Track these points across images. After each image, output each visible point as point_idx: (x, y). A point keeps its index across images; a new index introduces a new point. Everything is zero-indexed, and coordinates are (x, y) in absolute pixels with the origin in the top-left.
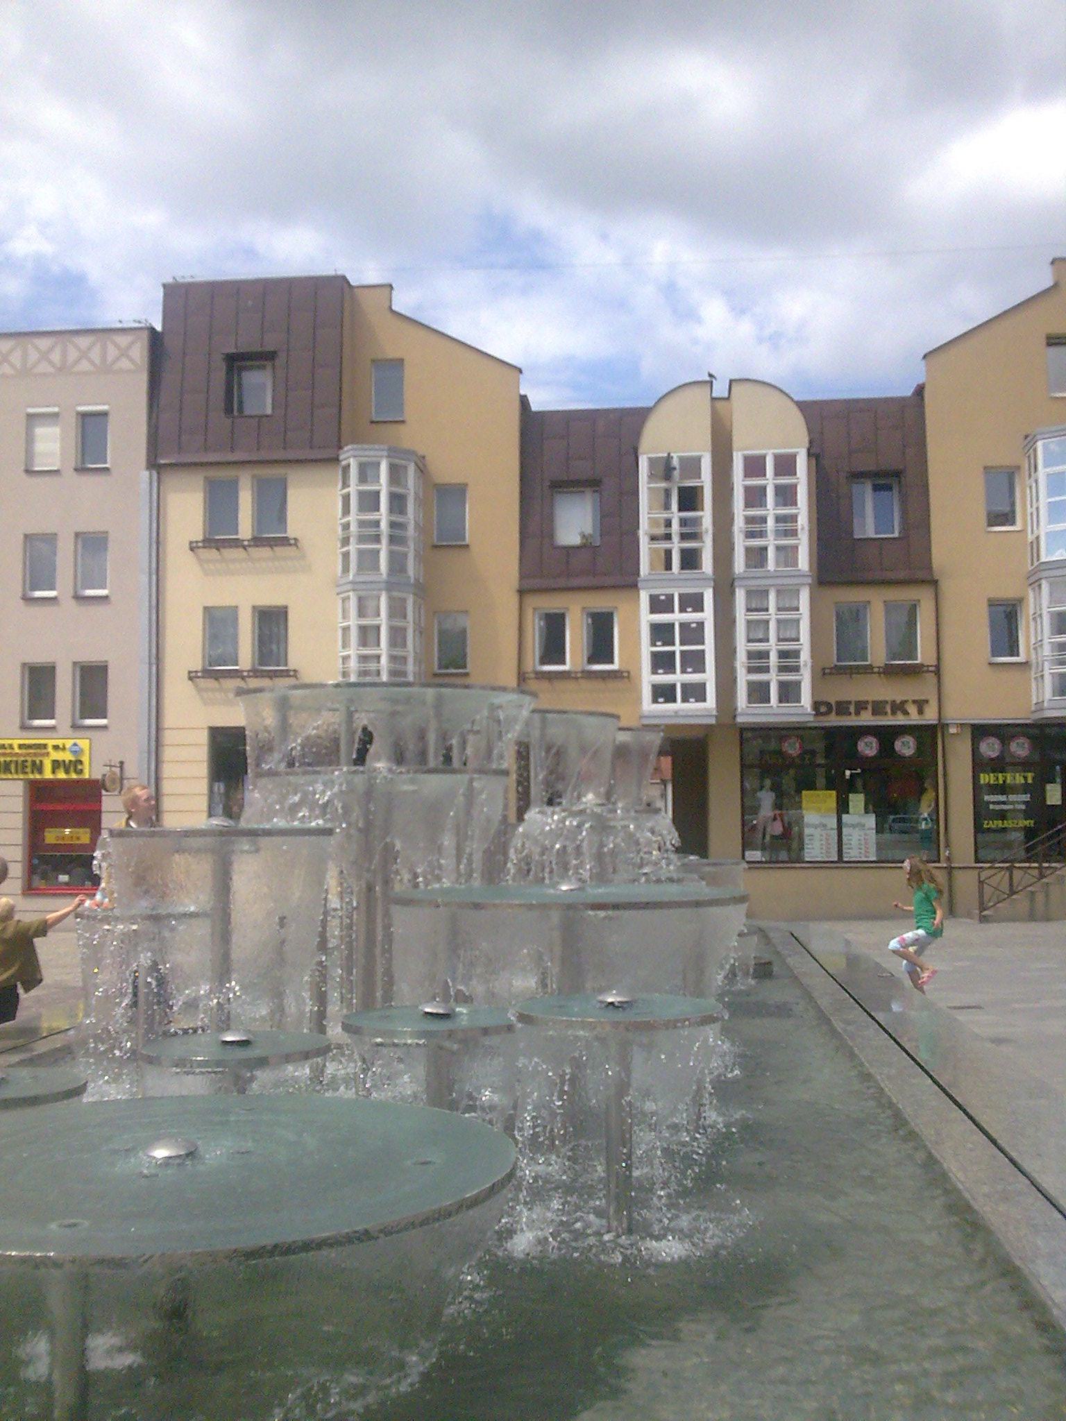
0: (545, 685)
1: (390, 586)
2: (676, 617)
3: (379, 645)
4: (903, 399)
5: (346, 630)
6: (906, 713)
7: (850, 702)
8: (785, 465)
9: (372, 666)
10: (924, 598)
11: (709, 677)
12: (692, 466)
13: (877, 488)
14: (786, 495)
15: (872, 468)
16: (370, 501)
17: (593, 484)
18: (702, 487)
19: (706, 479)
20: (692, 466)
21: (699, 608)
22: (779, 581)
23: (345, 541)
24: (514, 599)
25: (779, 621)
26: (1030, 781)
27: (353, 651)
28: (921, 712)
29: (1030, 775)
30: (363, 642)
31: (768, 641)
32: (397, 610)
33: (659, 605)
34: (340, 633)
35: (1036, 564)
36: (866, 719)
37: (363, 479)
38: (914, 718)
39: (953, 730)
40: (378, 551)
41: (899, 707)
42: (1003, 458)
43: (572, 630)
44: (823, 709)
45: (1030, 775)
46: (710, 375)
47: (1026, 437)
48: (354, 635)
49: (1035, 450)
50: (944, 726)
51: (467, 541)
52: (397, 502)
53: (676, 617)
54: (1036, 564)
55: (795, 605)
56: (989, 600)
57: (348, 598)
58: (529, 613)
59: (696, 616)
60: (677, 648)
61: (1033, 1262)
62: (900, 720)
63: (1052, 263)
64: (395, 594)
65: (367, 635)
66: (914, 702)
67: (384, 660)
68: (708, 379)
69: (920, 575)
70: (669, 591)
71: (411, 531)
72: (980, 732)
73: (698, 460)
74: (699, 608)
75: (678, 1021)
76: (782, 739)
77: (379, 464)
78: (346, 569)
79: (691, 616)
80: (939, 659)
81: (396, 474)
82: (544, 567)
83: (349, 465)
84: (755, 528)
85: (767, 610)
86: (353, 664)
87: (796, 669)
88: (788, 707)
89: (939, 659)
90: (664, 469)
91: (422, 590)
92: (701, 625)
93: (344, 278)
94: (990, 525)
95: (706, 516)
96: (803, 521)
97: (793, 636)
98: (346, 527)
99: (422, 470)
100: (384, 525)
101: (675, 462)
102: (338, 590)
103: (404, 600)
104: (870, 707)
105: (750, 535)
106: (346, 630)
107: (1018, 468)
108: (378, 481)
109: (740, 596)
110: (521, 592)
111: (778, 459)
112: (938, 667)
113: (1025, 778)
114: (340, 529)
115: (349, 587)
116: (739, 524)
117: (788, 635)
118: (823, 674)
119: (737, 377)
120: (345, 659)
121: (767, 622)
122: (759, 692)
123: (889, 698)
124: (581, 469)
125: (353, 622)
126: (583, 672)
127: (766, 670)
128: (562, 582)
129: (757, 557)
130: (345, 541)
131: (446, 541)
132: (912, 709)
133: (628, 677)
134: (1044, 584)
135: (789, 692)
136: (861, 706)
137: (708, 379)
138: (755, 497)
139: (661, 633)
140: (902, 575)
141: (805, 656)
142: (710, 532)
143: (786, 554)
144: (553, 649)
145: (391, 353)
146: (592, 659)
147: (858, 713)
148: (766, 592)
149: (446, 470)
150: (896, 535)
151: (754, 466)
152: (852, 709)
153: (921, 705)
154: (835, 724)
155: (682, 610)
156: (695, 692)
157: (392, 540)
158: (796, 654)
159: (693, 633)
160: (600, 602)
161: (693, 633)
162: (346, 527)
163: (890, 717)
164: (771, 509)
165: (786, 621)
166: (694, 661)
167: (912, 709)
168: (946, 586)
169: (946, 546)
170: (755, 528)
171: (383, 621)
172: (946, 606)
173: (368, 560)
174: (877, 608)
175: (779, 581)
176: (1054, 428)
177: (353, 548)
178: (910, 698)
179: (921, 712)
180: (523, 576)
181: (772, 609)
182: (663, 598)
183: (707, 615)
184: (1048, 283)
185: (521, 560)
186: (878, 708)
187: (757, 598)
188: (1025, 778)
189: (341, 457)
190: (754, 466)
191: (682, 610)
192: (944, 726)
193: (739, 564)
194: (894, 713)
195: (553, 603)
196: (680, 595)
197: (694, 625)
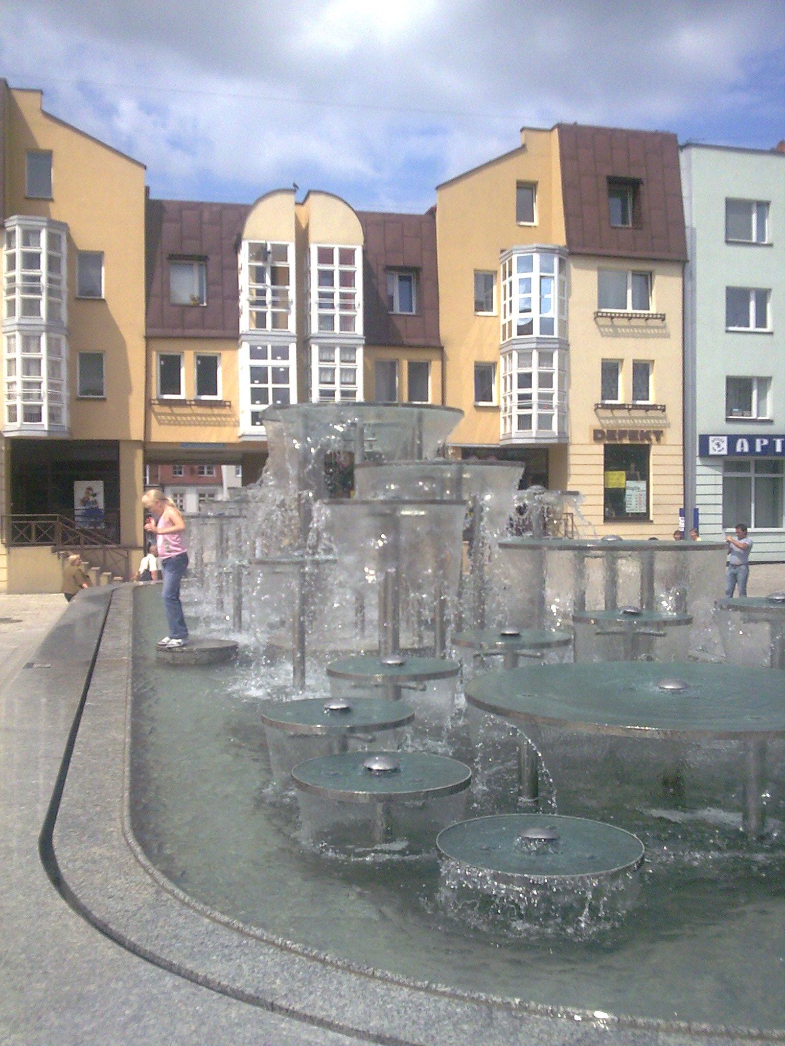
0: (166, 409)
1: (49, 329)
2: (269, 363)
3: (40, 375)
4: (420, 216)
5: (11, 361)
8: (347, 257)
9: (35, 391)
12: (281, 252)
13: (401, 279)
14: (347, 280)
15: (401, 264)
16: (31, 261)
17: (202, 259)
18: (288, 268)
19: (291, 262)
20: (281, 252)
21: (286, 357)
22: (250, 338)
23: (11, 291)
24: (142, 343)
25: (342, 370)
27: (19, 377)
30: (27, 372)
31: (333, 383)
32: (53, 349)
34: (5, 363)
35: (507, 339)
37: (26, 243)
40: (39, 301)
42: (487, 265)
43: (433, 378)
44: (600, 436)
46: (295, 185)
47: (502, 251)
48: (19, 365)
49: (510, 262)
51: (103, 297)
52: (53, 264)
54: (507, 339)
55: (353, 358)
56: (476, 362)
57: (14, 336)
58: (154, 354)
59: (284, 363)
63: (522, 130)
64: (52, 335)
65: (31, 365)
67: (44, 386)
68: (293, 187)
69: (434, 343)
70: (264, 344)
71: (64, 287)
73: (285, 248)
74: (286, 357)
77: (39, 232)
78: (11, 313)
79: (280, 363)
81: (53, 242)
82: (167, 323)
83: (15, 231)
85: (333, 361)
86: (18, 389)
87: (550, 407)
88: (545, 433)
90: (259, 252)
91: (70, 334)
92: (287, 369)
94: (476, 310)
95: (292, 289)
96: (359, 299)
98: (12, 280)
99: (70, 240)
100: (44, 280)
101: (269, 248)
102: (4, 330)
103: (58, 340)
106: (11, 361)
107: (496, 272)
108: (38, 244)
109: (315, 350)
110: (148, 338)
111: (342, 251)
114: (5, 282)
115: (16, 327)
116: (314, 299)
117: (348, 380)
119: (315, 188)
120: (10, 384)
121: (333, 370)
124: (191, 247)
125: (18, 355)
126: (195, 400)
127: (530, 407)
128: (178, 332)
130: (11, 291)
131: (87, 294)
133: (230, 406)
134: (515, 354)
137: (293, 187)
138: (326, 278)
139: (258, 374)
140: (421, 341)
142: (294, 303)
143: (347, 322)
144: (170, 381)
145: (43, 145)
146: (201, 392)
148: (334, 349)
149: (86, 241)
150: (414, 313)
151: (325, 256)
155: (274, 358)
157: (50, 292)
159: (281, 376)
160: (419, 356)
161: (281, 376)
162: (12, 280)
168: (448, 351)
171: (43, 354)
172: (448, 364)
173: (31, 308)
175: (342, 341)
176: (525, 247)
177: (18, 296)
180: (148, 326)
182: (259, 348)
183: (292, 363)
185: (146, 314)
187: (326, 350)
189: (7, 224)
190: (325, 256)
191: (274, 358)
193: (314, 328)
195: (170, 348)
196: (273, 347)
197: (282, 370)
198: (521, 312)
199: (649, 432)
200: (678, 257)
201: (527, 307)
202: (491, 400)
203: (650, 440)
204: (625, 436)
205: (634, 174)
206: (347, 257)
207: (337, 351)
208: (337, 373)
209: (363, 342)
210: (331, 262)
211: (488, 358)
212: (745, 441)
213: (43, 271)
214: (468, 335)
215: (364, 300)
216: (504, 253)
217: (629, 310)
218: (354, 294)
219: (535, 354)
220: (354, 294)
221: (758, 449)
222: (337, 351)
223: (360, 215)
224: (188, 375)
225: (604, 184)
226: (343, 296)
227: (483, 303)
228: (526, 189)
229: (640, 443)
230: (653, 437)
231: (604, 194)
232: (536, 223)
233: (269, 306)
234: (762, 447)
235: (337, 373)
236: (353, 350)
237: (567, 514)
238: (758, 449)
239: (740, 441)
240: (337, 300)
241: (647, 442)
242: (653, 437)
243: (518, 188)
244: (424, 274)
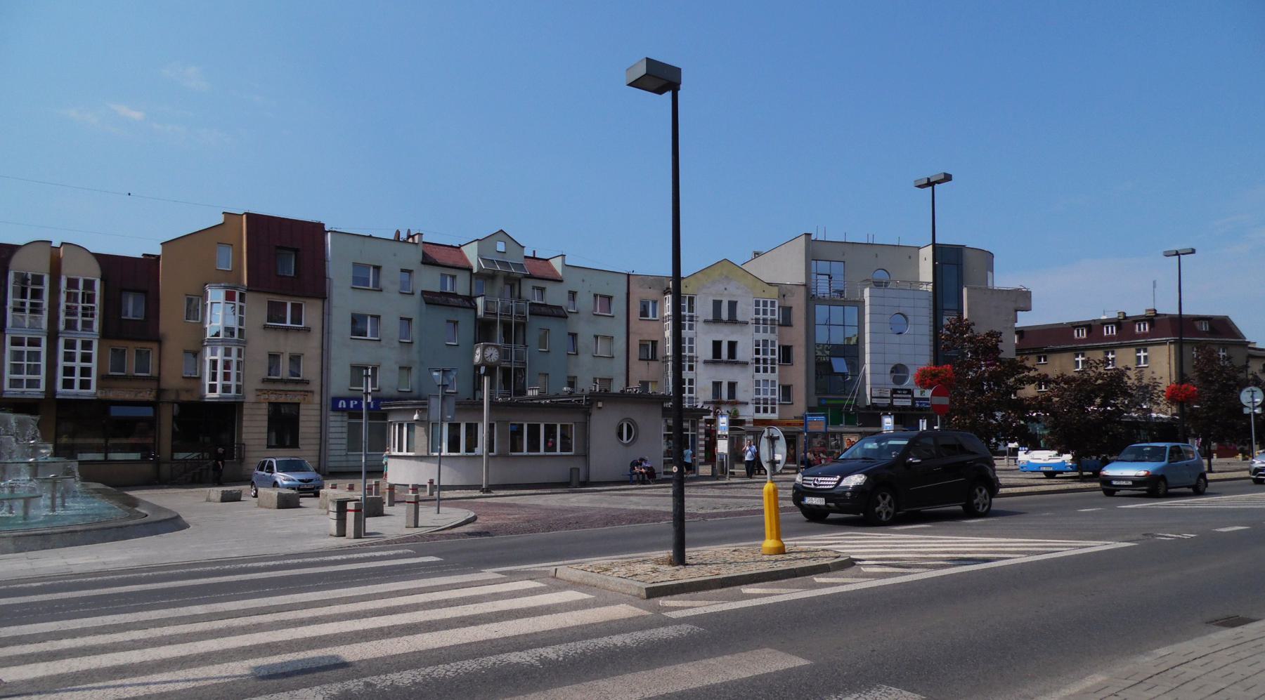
10: (155, 346)
11: (42, 377)
12: (38, 279)
33: (17, 342)
53: (25, 376)
60: (25, 363)
61: (230, 331)
84: (69, 371)
90: (22, 279)
101: (30, 277)
105: (66, 360)
109: (61, 342)
118: (103, 378)
122: (68, 384)
129: (70, 325)
135: (85, 385)
138: (69, 357)
156: (33, 384)
164: (78, 364)
166: (35, 370)
169: (165, 325)
170: (70, 311)
174: (131, 349)
183: (43, 349)
184: (221, 221)
193: (62, 327)
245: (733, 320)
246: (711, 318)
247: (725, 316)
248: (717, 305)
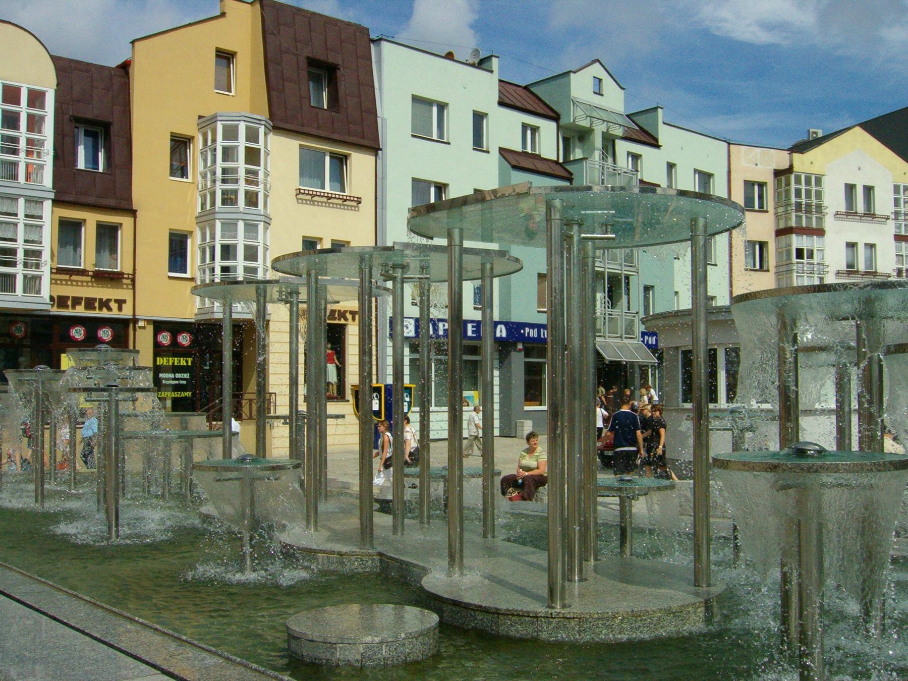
4: (109, 69)
6: (109, 309)
7: (68, 298)
8: (36, 98)
10: (126, 221)
14: (35, 123)
26: (190, 364)
28: (120, 309)
29: (190, 360)
36: (80, 311)
38: (115, 314)
39: (141, 324)
41: (105, 304)
45: (190, 360)
50: (135, 321)
56: (303, 237)
62: (104, 314)
66: (116, 301)
69: (124, 204)
72: (159, 326)
75: (710, 388)
76: (13, 323)
80: (134, 270)
89: (134, 270)
93: (802, 153)
97: (9, 236)
104: (83, 303)
112: (134, 274)
113: (187, 362)
121: (16, 225)
123: (98, 297)
127: (14, 264)
132: (114, 306)
136: (77, 301)
141: (46, 256)
147: (74, 307)
152: (70, 303)
153: (120, 303)
154: (56, 313)
158: (38, 254)
163: (70, 309)
165: (31, 226)
167: (114, 306)
178: (113, 297)
179: (120, 309)
181: (21, 215)
186: (90, 303)
188: (187, 362)
192: (135, 321)
194: (100, 309)
198: (183, 173)
199: (346, 312)
200: (372, 145)
201: (783, 238)
202: (185, 272)
203: (346, 319)
204: (80, 304)
205: (331, 59)
206: (36, 98)
207: (21, 201)
208: (21, 228)
209: (52, 196)
210: (17, 102)
211: (181, 226)
212: (503, 327)
213: (220, 143)
214: (161, 199)
215: (55, 149)
216: (202, 120)
217: (327, 189)
218: (44, 141)
219: (241, 225)
220: (44, 141)
221: (441, 333)
222: (21, 201)
223: (55, 59)
224: (88, 235)
225: (303, 63)
226: (30, 142)
227: (179, 168)
228: (225, 57)
229: (337, 322)
230: (349, 316)
231: (304, 74)
232: (233, 93)
233: (22, 155)
234: (445, 330)
235: (21, 228)
236: (39, 202)
237: (271, 394)
238: (441, 333)
239: (499, 327)
240: (23, 145)
241: (342, 321)
242: (349, 316)
243: (217, 56)
244: (114, 129)
245: (870, 214)
246: (843, 208)
247: (860, 207)
248: (850, 189)
